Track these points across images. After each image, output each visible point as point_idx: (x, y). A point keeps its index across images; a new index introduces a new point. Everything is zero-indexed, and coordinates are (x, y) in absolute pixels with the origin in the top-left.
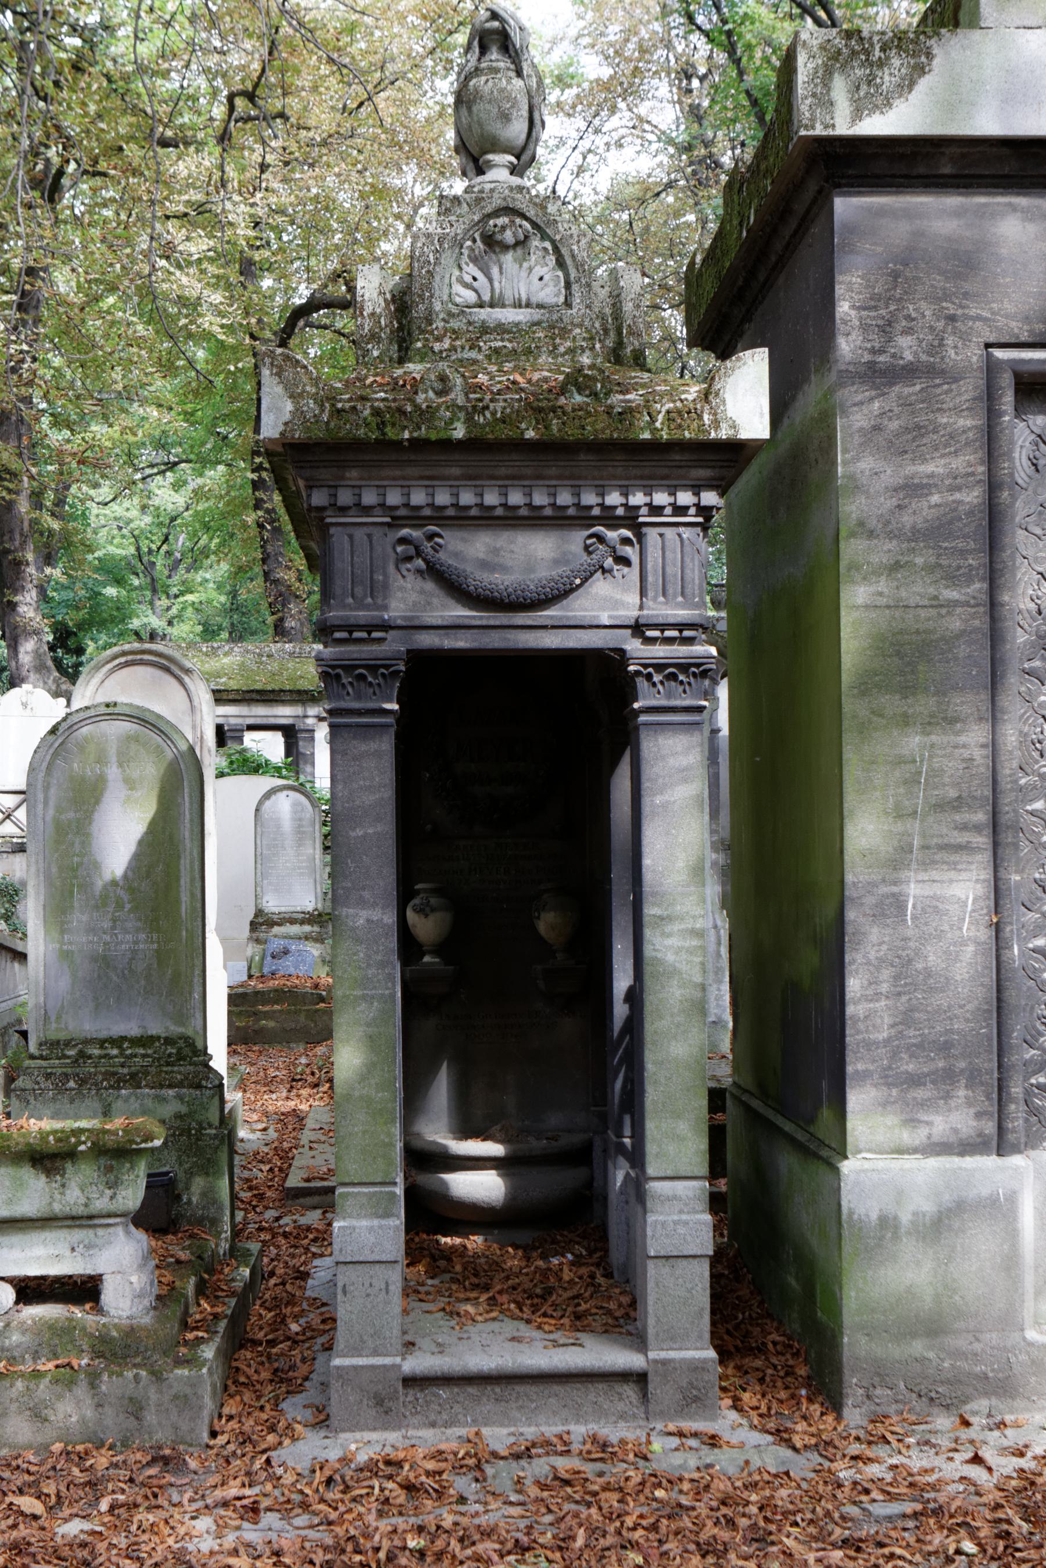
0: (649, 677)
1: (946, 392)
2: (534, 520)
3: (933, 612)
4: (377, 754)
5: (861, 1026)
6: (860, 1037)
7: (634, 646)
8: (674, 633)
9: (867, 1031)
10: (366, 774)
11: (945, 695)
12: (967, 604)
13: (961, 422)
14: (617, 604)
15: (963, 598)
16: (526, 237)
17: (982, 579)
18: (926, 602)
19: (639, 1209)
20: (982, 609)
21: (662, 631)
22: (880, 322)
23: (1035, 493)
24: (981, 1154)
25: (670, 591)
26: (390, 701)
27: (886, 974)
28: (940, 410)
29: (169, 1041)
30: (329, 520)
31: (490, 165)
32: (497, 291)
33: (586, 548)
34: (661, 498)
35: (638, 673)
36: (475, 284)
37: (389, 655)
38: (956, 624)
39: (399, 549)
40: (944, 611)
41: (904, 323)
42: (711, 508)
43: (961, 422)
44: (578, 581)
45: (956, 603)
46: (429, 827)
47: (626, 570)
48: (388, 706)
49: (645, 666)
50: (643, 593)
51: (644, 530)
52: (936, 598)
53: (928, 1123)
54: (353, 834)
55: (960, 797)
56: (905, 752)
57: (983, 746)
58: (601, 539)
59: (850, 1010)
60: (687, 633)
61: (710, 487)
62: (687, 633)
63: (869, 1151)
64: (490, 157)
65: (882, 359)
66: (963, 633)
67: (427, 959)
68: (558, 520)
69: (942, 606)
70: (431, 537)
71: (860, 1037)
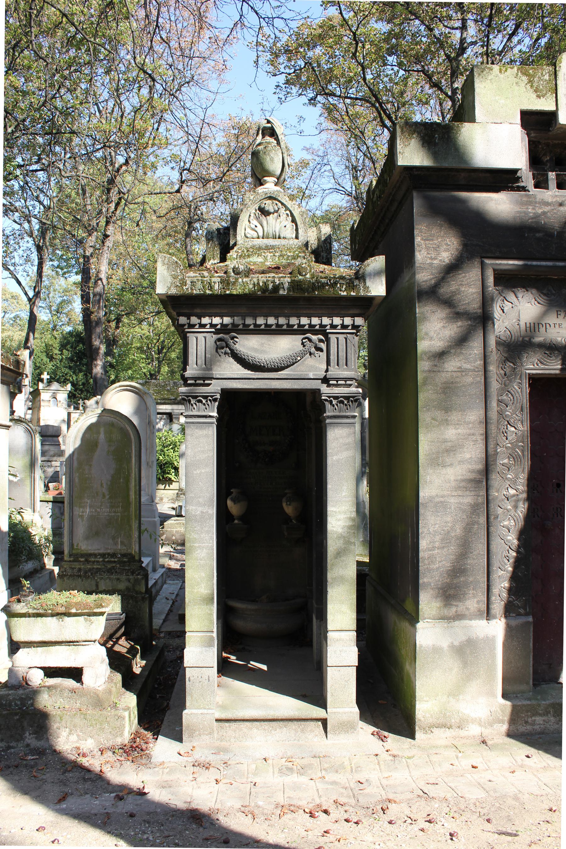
0: (331, 402)
1: (464, 277)
2: (279, 331)
3: (459, 374)
4: (207, 436)
5: (426, 562)
6: (425, 567)
7: (324, 389)
8: (343, 382)
9: (429, 564)
10: (202, 445)
11: (464, 411)
12: (474, 371)
13: (471, 290)
14: (316, 369)
15: (472, 368)
16: (279, 209)
17: (481, 360)
18: (456, 370)
19: (324, 642)
20: (481, 373)
21: (346, 381)
22: (434, 246)
23: (503, 322)
24: (479, 619)
25: (340, 363)
26: (213, 411)
27: (438, 538)
28: (461, 284)
29: (124, 555)
30: (187, 330)
31: (266, 182)
32: (266, 232)
33: (303, 343)
34: (337, 321)
35: (326, 400)
36: (256, 229)
37: (213, 391)
38: (469, 379)
39: (218, 343)
40: (464, 374)
41: (445, 247)
42: (359, 326)
43: (471, 290)
44: (299, 358)
45: (469, 370)
46: (237, 465)
47: (321, 353)
48: (212, 414)
49: (329, 397)
50: (328, 363)
51: (330, 335)
52: (460, 368)
53: (457, 606)
54: (195, 472)
55: (471, 458)
56: (447, 437)
57: (481, 435)
58: (310, 340)
59: (421, 554)
60: (348, 382)
61: (358, 316)
62: (348, 382)
63: (429, 618)
64: (265, 178)
65: (435, 262)
66: (472, 383)
67: (236, 521)
68: (290, 331)
69: (463, 371)
70: (232, 338)
71: (425, 567)
